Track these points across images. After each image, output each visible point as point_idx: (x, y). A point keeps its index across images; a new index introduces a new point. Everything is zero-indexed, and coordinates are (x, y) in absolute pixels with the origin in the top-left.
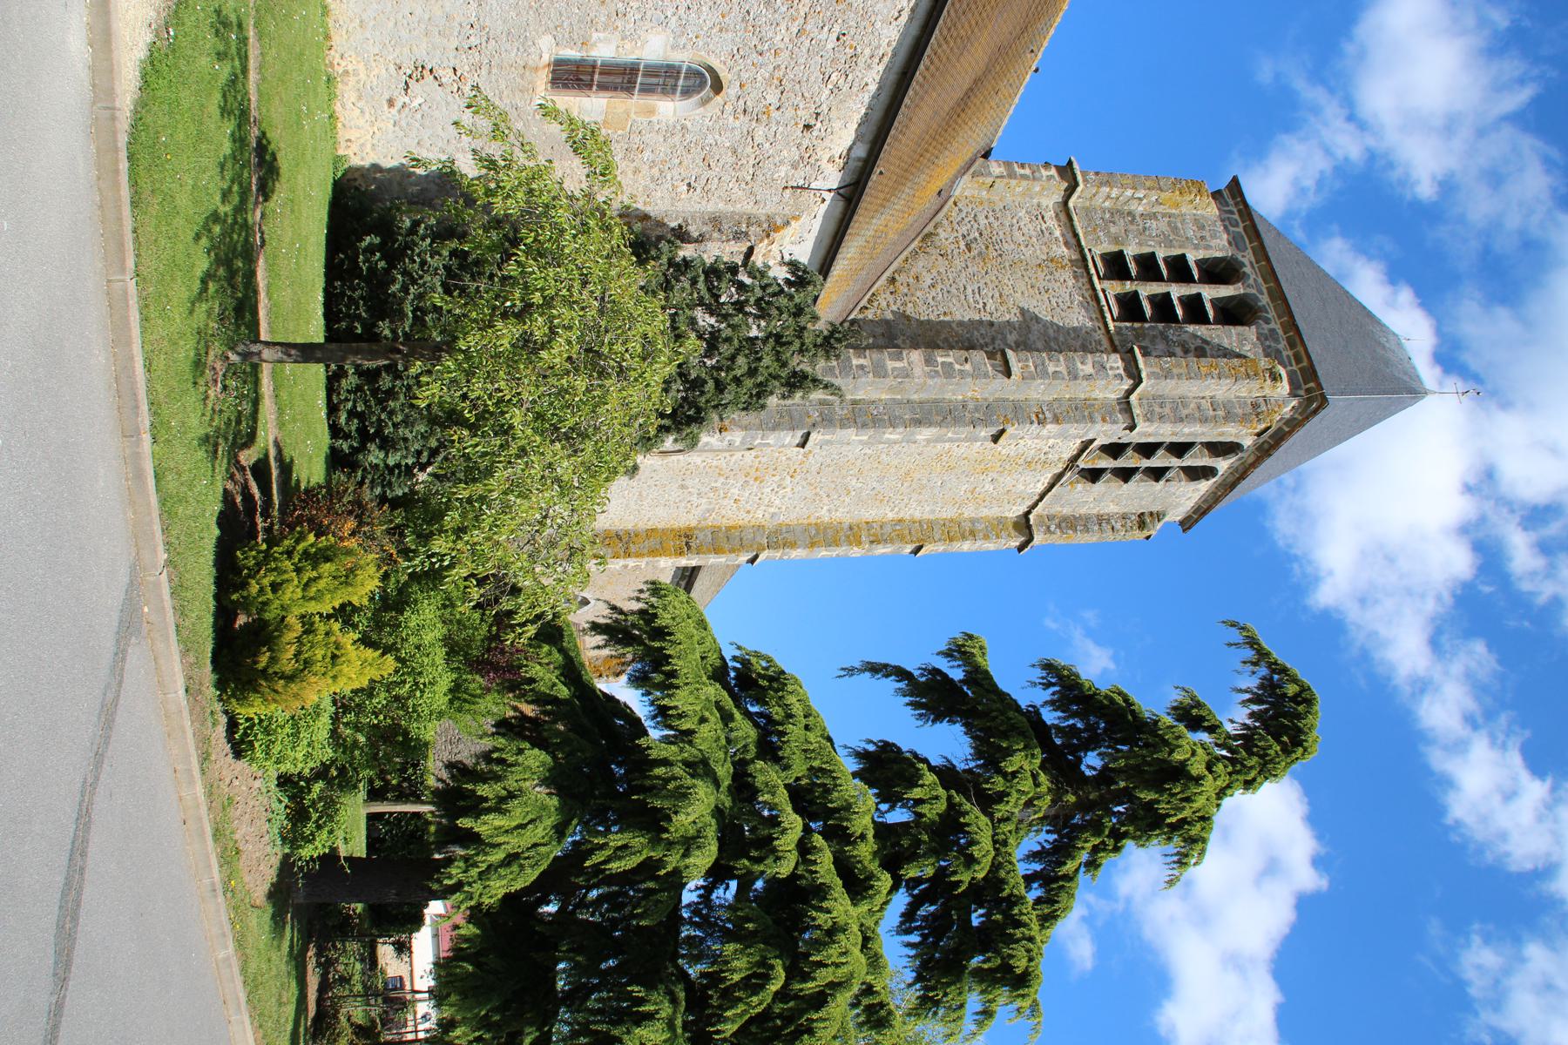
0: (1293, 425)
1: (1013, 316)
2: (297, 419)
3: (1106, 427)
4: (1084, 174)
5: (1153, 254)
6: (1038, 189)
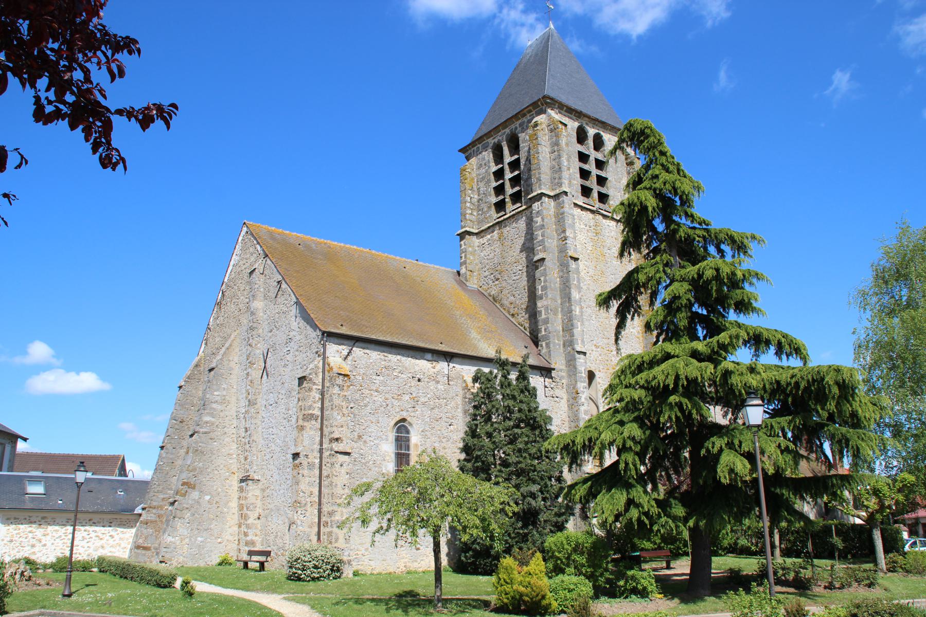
1: (524, 255)
4: (462, 228)
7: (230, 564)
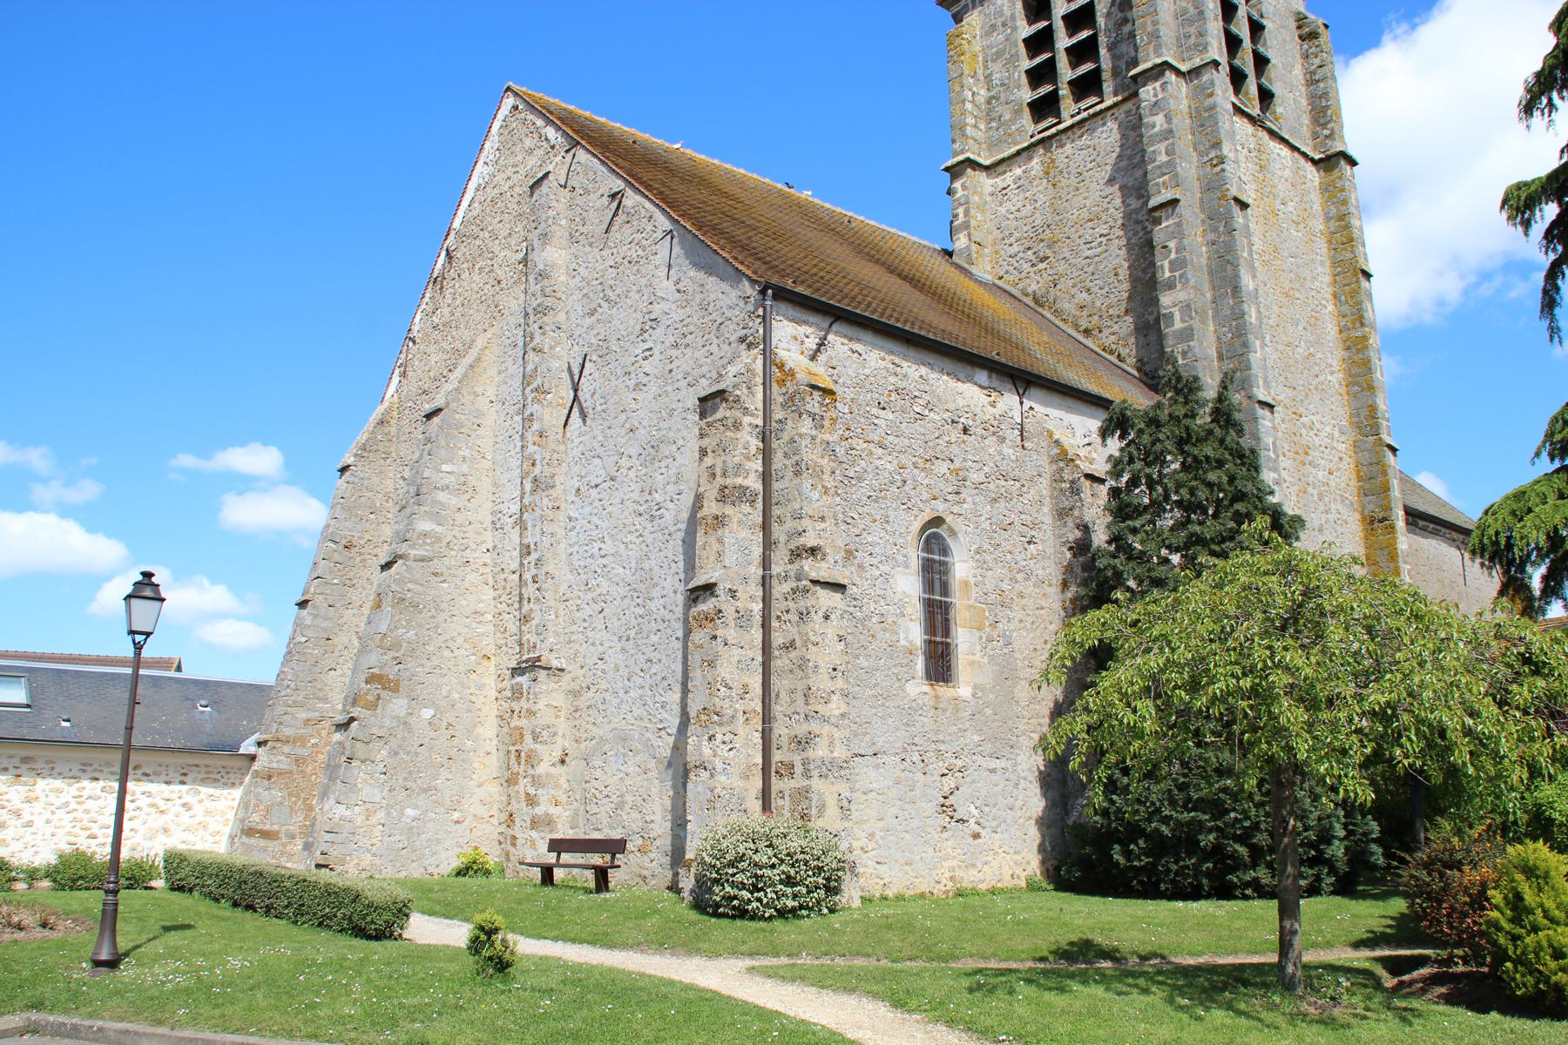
2: (1337, 928)
4: (956, 154)
5: (1027, 72)
6: (976, 198)
7: (487, 873)
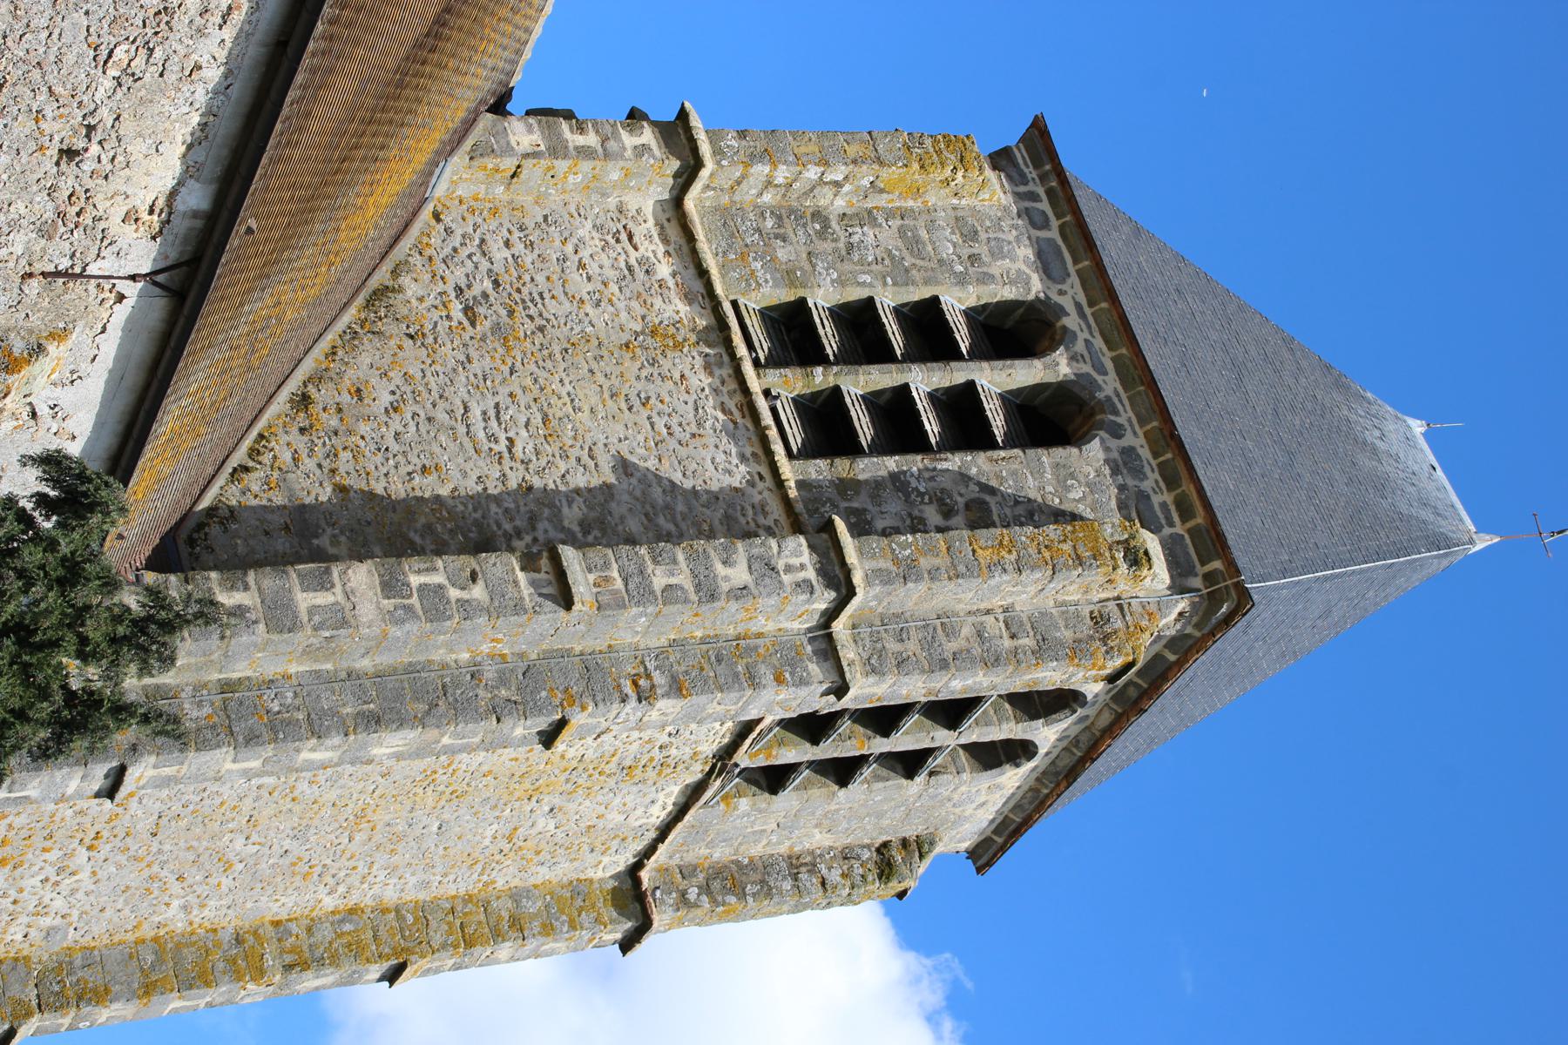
0: (1182, 650)
3: (784, 694)
4: (714, 136)
5: (871, 300)
